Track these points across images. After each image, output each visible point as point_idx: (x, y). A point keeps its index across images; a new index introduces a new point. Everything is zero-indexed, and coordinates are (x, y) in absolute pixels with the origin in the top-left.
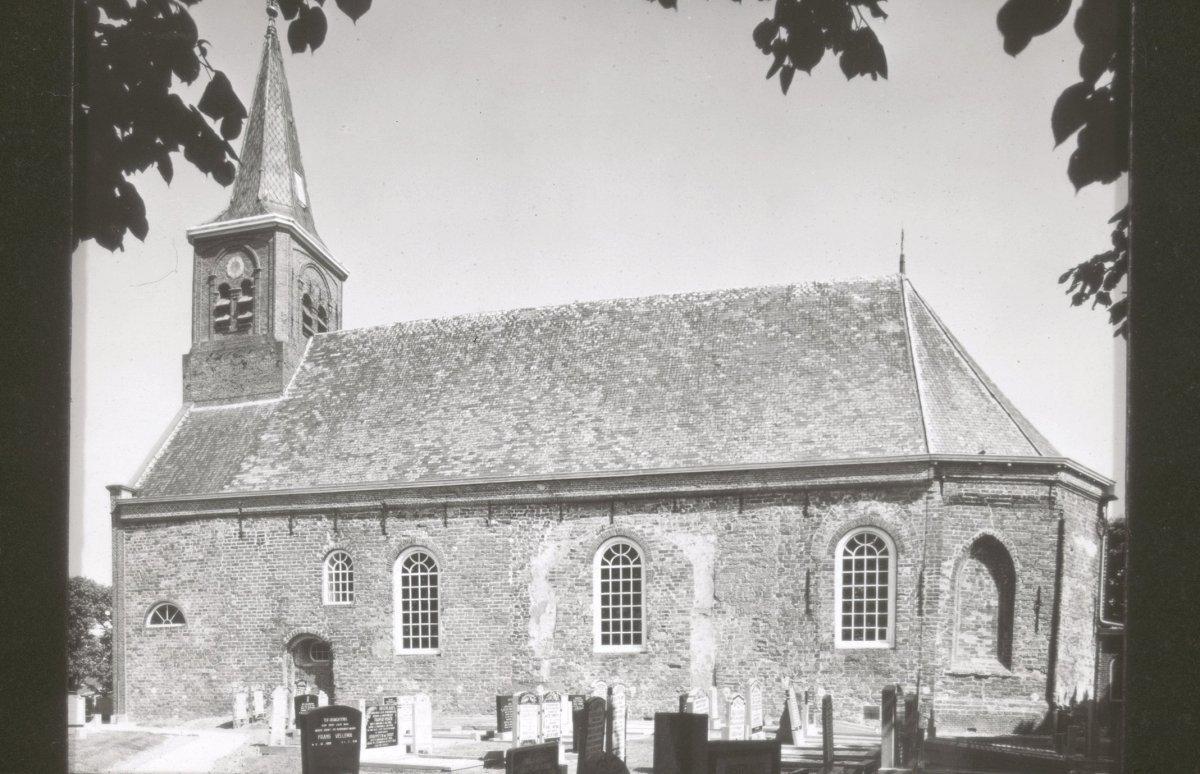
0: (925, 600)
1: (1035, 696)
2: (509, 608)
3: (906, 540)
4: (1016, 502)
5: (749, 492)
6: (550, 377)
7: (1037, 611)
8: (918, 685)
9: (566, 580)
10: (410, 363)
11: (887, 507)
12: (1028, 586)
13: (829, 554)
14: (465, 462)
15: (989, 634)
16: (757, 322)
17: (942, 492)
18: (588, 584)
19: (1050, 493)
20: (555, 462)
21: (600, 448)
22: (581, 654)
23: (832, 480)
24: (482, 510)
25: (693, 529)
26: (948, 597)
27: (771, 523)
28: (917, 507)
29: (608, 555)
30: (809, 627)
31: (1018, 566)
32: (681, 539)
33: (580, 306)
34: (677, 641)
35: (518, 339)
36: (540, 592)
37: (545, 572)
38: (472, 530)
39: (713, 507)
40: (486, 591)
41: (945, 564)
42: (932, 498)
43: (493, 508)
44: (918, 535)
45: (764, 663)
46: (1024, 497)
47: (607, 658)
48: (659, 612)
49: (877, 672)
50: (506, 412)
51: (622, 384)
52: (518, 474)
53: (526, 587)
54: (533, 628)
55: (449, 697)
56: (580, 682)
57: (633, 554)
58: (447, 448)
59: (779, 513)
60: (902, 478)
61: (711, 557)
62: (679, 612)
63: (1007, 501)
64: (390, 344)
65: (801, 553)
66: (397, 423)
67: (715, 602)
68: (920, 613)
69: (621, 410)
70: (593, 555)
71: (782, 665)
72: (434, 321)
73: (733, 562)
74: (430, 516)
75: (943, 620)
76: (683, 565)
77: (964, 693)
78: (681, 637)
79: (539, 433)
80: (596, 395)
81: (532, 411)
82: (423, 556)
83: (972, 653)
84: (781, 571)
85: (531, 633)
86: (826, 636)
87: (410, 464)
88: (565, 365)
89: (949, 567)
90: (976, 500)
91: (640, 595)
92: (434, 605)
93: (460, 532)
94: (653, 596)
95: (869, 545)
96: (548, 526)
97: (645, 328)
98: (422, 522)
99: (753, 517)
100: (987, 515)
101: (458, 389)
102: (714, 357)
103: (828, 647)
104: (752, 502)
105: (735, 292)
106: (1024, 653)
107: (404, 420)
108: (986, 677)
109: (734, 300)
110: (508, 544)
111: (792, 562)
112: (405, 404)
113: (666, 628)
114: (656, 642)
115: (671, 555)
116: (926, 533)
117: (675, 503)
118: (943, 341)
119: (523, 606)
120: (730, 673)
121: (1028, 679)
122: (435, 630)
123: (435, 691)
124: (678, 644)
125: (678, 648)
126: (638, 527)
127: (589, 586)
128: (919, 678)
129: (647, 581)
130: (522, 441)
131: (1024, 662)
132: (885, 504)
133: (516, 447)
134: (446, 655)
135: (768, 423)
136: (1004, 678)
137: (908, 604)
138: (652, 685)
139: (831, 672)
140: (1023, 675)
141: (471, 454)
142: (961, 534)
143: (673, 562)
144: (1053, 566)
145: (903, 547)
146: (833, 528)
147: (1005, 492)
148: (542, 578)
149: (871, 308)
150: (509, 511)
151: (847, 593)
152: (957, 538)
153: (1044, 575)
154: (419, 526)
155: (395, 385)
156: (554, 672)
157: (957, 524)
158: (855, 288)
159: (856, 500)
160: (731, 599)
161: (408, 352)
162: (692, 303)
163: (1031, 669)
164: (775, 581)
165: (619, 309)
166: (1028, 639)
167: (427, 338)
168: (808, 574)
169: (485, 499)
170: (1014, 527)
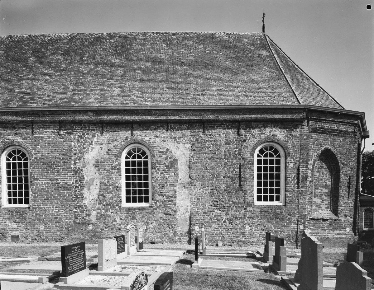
0: (300, 180)
1: (348, 229)
2: (72, 181)
3: (290, 149)
4: (340, 133)
5: (209, 121)
6: (94, 63)
7: (349, 187)
8: (297, 225)
9: (105, 166)
10: (15, 53)
11: (281, 132)
12: (345, 175)
13: (251, 156)
14: (46, 100)
15: (326, 198)
16: (199, 46)
17: (308, 125)
18: (118, 169)
20: (98, 101)
21: (124, 96)
22: (115, 207)
23: (253, 116)
24: (55, 126)
25: (178, 140)
26: (310, 179)
27: (220, 139)
28: (296, 133)
29: (129, 154)
31: (341, 165)
32: (171, 145)
33: (109, 34)
34: (169, 201)
35: (76, 46)
36: (90, 173)
37: (93, 162)
38: (49, 137)
39: (188, 129)
40: (58, 171)
41: (309, 163)
42: (304, 128)
43: (61, 125)
44: (296, 147)
45: (217, 213)
47: (129, 210)
48: (159, 185)
49: (276, 218)
50: (70, 77)
51: (133, 68)
52: (77, 106)
53: (82, 170)
54: (86, 193)
55: (35, 232)
56: (114, 223)
57: (144, 153)
58: (34, 93)
59: (224, 133)
60: (290, 116)
61: (188, 156)
62: (170, 185)
63: (336, 132)
64: (4, 44)
65: (236, 155)
66: (6, 80)
67: (190, 180)
68: (298, 187)
69: (134, 79)
70: (121, 153)
71: (226, 214)
72: (30, 36)
73: (200, 159)
74: (23, 128)
75: (308, 191)
76: (172, 160)
77: (317, 228)
78: (171, 198)
79: (89, 88)
80: (120, 72)
81: (84, 78)
82: (19, 152)
83: (319, 208)
84: (226, 164)
85: (85, 196)
86: (250, 199)
87: (11, 100)
88: (102, 58)
89: (311, 164)
90: (322, 131)
91: (148, 175)
92: (26, 179)
93: (42, 138)
94: (155, 176)
95: (18, 155)
96: (95, 136)
97: (144, 45)
98: (18, 131)
99: (210, 135)
100: (327, 139)
101: (42, 66)
102: (180, 59)
103: (251, 204)
104: (210, 127)
105: (187, 33)
106: (343, 208)
107: (10, 79)
108: (327, 220)
109: (186, 37)
110: (71, 145)
111: (232, 159)
112: (11, 72)
113: (163, 194)
114: (157, 201)
115: (166, 154)
116: (301, 146)
117: (168, 126)
118: (289, 61)
119: (80, 180)
120: (198, 218)
121: (345, 221)
122: (27, 194)
123: (27, 228)
124: (170, 203)
125: (170, 204)
126: (147, 138)
127: (119, 170)
128: (298, 221)
129: (152, 168)
130: (79, 91)
131: (343, 212)
132: (280, 130)
133: (76, 94)
134: (33, 208)
135: (214, 89)
136: (335, 220)
137: (292, 183)
138: (155, 225)
139: (253, 218)
140: (343, 219)
141: (48, 96)
142: (316, 147)
143: (166, 158)
145: (289, 153)
146: (253, 142)
147: (336, 128)
148: (92, 165)
149: (253, 45)
150: (72, 127)
151: (259, 177)
152: (314, 150)
153: (351, 170)
154: (16, 134)
155: (6, 63)
156: (98, 218)
157: (314, 143)
158: (245, 36)
159: (265, 127)
160: (198, 178)
161: (15, 48)
162: (166, 36)
163: (346, 216)
164: (223, 169)
165: (129, 36)
166: (345, 201)
167: (26, 43)
168: (240, 166)
169: (57, 119)
170: (339, 146)
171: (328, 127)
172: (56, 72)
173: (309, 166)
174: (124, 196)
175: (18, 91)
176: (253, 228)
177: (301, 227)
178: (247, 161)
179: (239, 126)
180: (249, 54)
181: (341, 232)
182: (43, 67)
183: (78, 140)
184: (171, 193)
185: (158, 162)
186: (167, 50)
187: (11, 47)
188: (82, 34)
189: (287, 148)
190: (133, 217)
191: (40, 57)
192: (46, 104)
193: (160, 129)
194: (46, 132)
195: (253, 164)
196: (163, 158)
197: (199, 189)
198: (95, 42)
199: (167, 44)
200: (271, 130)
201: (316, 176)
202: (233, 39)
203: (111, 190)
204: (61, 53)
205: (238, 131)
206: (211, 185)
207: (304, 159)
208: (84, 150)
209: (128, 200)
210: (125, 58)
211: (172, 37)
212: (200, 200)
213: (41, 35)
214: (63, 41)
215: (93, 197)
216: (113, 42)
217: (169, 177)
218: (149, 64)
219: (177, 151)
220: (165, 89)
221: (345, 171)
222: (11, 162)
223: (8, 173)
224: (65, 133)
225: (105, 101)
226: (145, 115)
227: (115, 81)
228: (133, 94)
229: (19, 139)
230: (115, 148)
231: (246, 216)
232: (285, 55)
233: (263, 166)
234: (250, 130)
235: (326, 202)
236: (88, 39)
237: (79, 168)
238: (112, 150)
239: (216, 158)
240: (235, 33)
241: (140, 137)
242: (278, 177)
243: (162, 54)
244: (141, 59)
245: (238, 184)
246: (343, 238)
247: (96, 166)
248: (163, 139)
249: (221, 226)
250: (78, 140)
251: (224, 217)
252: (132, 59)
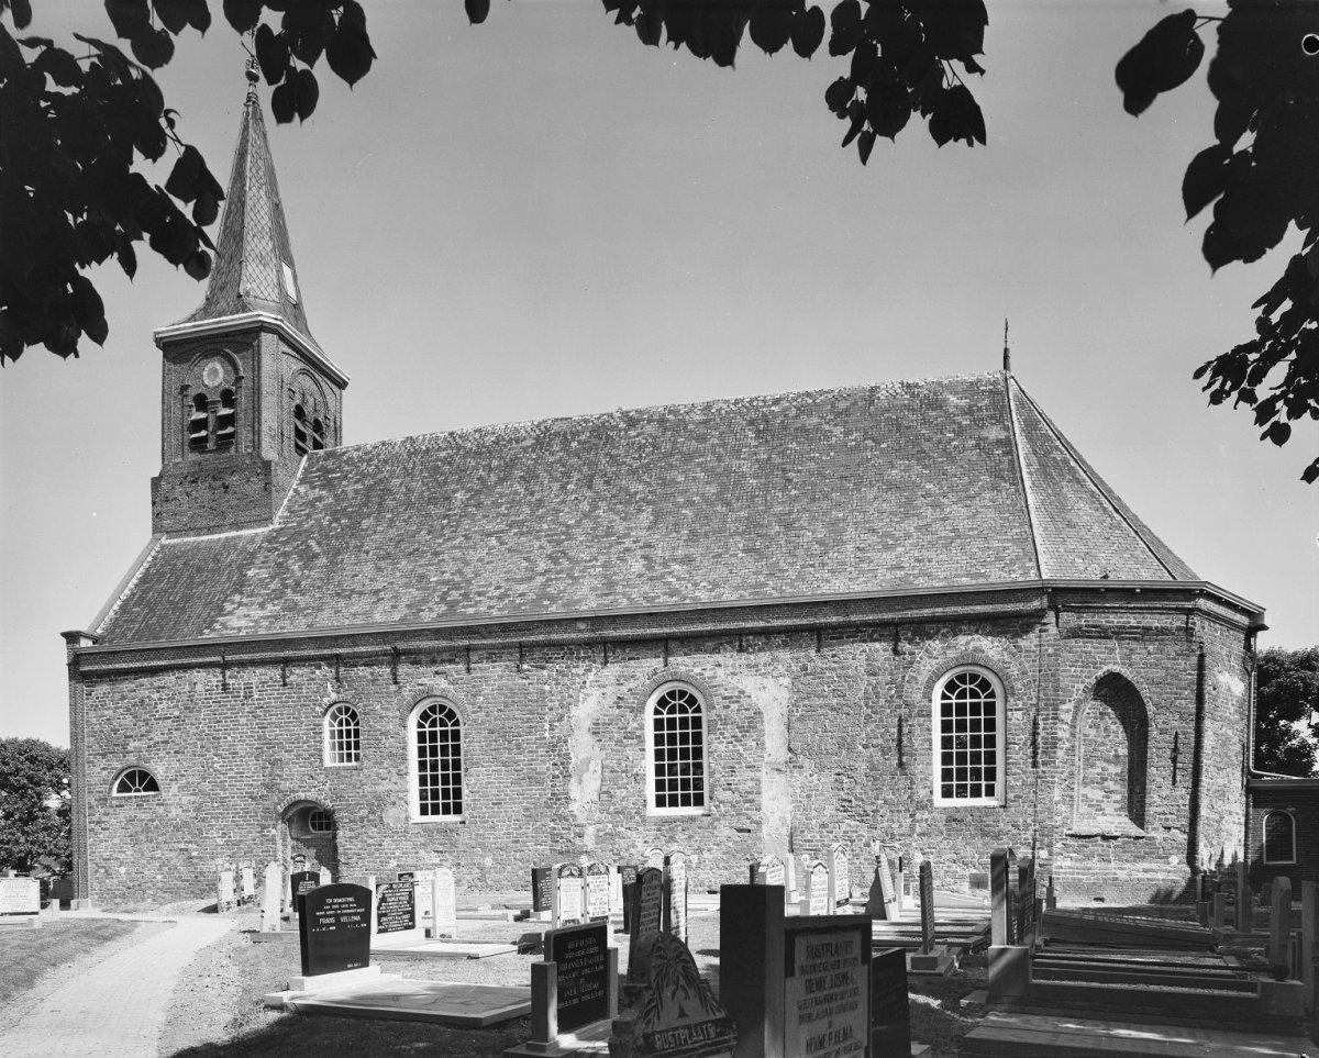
1: (1174, 860)
3: (1016, 680)
4: (1146, 634)
7: (1174, 760)
8: (1033, 849)
14: (491, 598)
15: (1118, 787)
19: (1187, 623)
21: (651, 579)
23: (927, 612)
26: (1068, 745)
27: (856, 663)
28: (1029, 641)
29: (662, 702)
30: (903, 782)
31: (1151, 709)
32: (748, 683)
34: (746, 802)
35: (552, 454)
36: (582, 747)
37: (588, 724)
38: (501, 677)
39: (785, 645)
40: (518, 746)
43: (524, 650)
44: (1030, 674)
46: (1156, 628)
47: (664, 822)
48: (724, 768)
49: (984, 834)
50: (538, 539)
52: (555, 610)
54: (574, 790)
56: (632, 850)
58: (469, 582)
59: (864, 651)
60: (1009, 607)
61: (785, 703)
63: (1136, 633)
65: (892, 697)
66: (410, 554)
68: (1035, 765)
69: (674, 535)
70: (645, 703)
72: (451, 434)
73: (811, 709)
74: (451, 661)
77: (1089, 857)
78: (750, 796)
79: (578, 562)
80: (646, 517)
81: (570, 537)
82: (443, 708)
85: (572, 795)
86: (922, 793)
87: (424, 601)
89: (1068, 711)
92: (457, 765)
94: (715, 749)
95: (972, 686)
97: (702, 439)
99: (834, 656)
101: (482, 512)
102: (784, 470)
103: (926, 805)
105: (808, 394)
106: (1159, 810)
107: (417, 550)
108: (1115, 838)
109: (807, 404)
110: (542, 692)
113: (733, 787)
116: (1040, 671)
117: (741, 641)
118: (1057, 448)
119: (562, 764)
121: (1165, 839)
123: (459, 864)
124: (747, 805)
125: (747, 809)
126: (697, 670)
127: (641, 739)
128: (1035, 840)
132: (990, 638)
136: (1137, 838)
137: (1020, 754)
139: (929, 835)
140: (1159, 835)
144: (1192, 708)
145: (1012, 687)
147: (1133, 623)
149: (970, 411)
151: (946, 743)
154: (437, 673)
156: (599, 840)
158: (952, 388)
160: (809, 751)
161: (421, 471)
162: (757, 409)
165: (671, 417)
167: (443, 454)
168: (900, 720)
171: (1112, 622)
172: (510, 526)
173: (1063, 716)
174: (651, 793)
175: (435, 579)
176: (931, 856)
177: (1043, 854)
178: (916, 710)
179: (897, 634)
180: (953, 440)
181: (1154, 866)
182: (484, 516)
183: (557, 679)
184: (750, 784)
185: (721, 720)
186: (757, 447)
187: (413, 469)
188: (566, 419)
189: (1008, 677)
190: (671, 837)
191: (476, 491)
192: (493, 607)
193: (725, 649)
194: (494, 667)
195: (929, 715)
196: (732, 711)
197: (811, 775)
198: (594, 441)
199: (758, 432)
200: (970, 638)
201: (1088, 736)
202: (921, 401)
203: (625, 781)
204: (521, 477)
205: (896, 645)
206: (835, 765)
207: (1048, 700)
208: (569, 700)
209: (660, 802)
210: (660, 478)
211: (773, 408)
212: (813, 798)
213: (475, 431)
214: (524, 444)
215: (588, 798)
216: (634, 437)
217: (745, 750)
218: (712, 490)
219: (762, 694)
220: (740, 555)
221: (1164, 723)
222: (427, 729)
223: (422, 752)
224: (532, 666)
225: (610, 594)
226: (692, 622)
227: (634, 542)
228: (670, 573)
229: (442, 683)
230: (633, 694)
231: (914, 831)
232: (1050, 432)
233: (968, 717)
234: (923, 640)
235: (1119, 797)
236: (578, 433)
237: (560, 738)
238: (626, 697)
239: (847, 705)
240: (930, 379)
241: (683, 669)
242: (991, 741)
243: (745, 459)
244: (694, 479)
245: (896, 761)
246: (1158, 880)
247: (594, 733)
248: (731, 669)
249: (857, 855)
250: (557, 679)
251: (864, 831)
252: (673, 481)
